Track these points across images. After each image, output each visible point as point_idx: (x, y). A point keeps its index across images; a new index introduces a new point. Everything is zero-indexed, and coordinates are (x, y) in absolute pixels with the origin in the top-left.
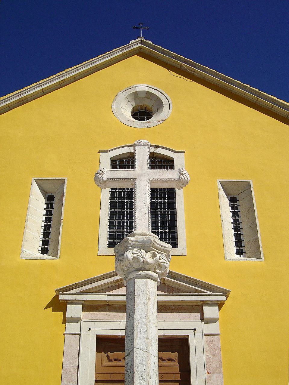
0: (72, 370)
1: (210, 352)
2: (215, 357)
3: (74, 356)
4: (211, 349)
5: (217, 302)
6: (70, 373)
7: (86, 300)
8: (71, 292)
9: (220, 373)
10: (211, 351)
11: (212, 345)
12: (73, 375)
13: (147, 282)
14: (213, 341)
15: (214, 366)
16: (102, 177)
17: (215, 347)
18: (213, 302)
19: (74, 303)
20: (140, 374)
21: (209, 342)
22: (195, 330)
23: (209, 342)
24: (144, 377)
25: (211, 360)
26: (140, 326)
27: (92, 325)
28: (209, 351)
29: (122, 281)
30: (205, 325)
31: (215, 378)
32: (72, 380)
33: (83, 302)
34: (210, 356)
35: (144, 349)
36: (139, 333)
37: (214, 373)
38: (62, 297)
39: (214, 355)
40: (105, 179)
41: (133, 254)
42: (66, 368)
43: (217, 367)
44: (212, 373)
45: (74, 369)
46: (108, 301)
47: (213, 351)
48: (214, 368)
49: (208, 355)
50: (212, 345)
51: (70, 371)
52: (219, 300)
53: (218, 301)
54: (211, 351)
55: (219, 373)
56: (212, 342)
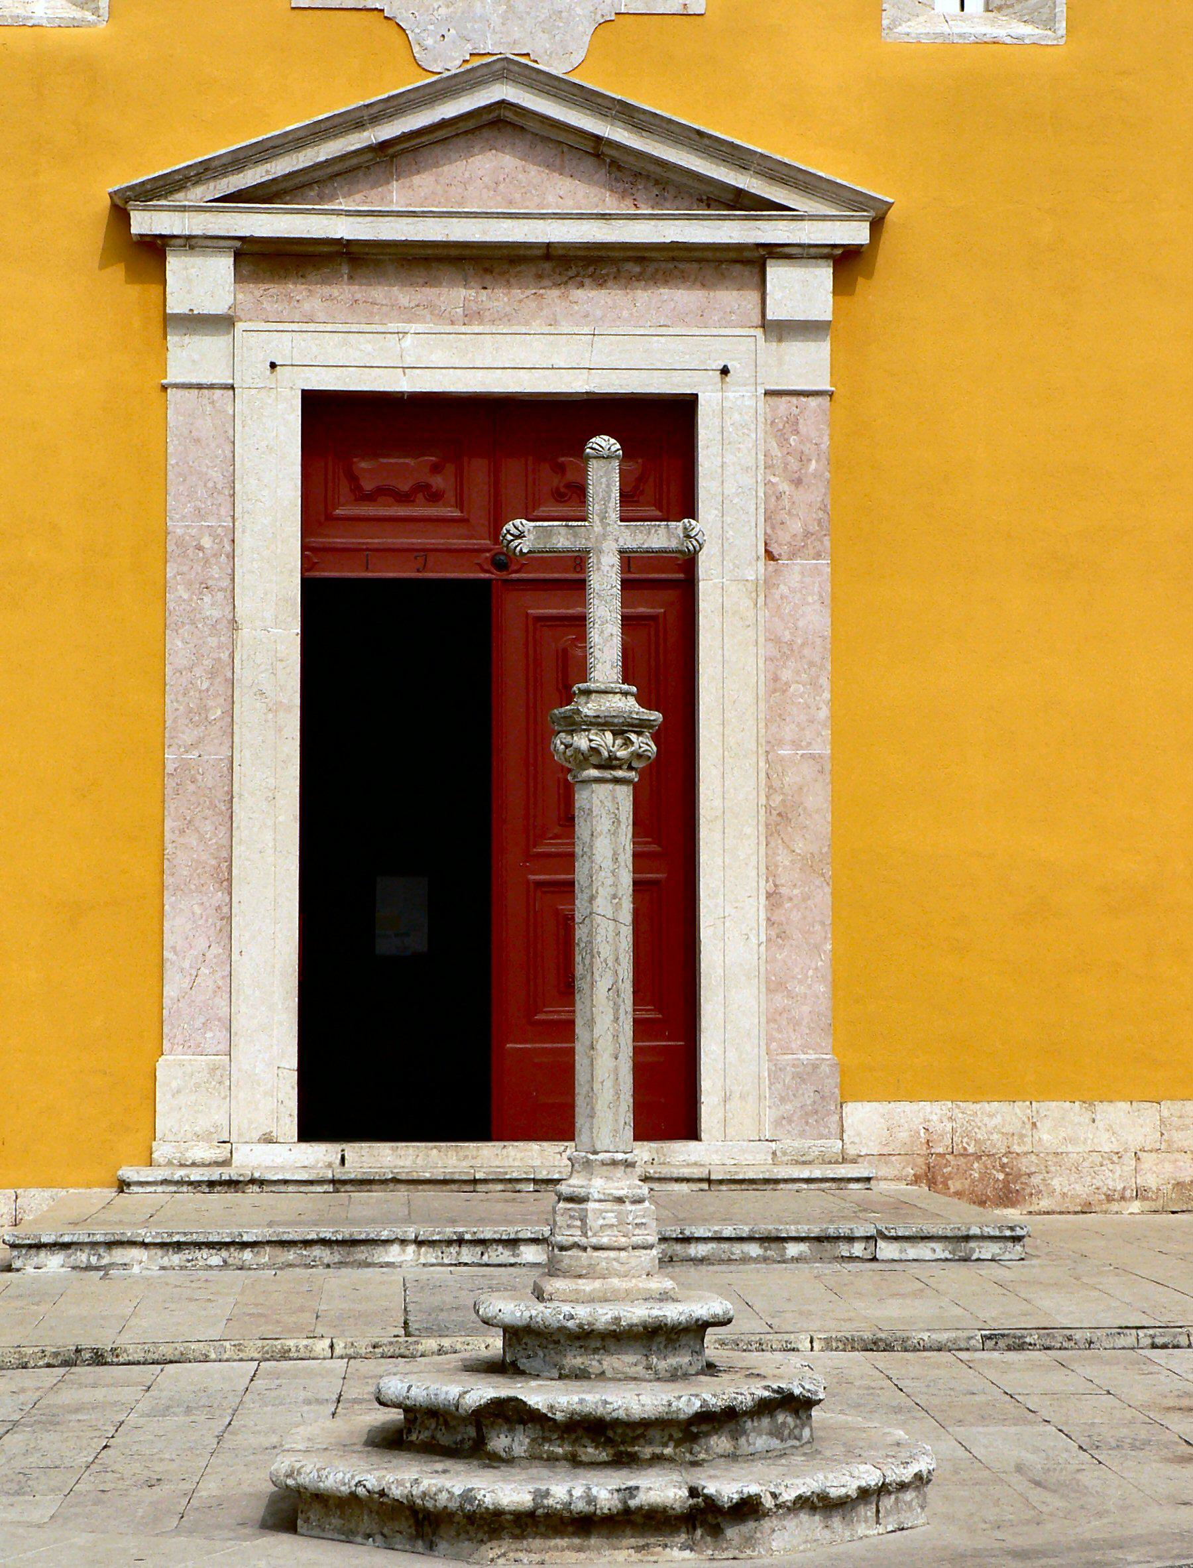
0: (206, 542)
1: (785, 469)
2: (801, 489)
3: (210, 484)
4: (789, 458)
5: (826, 251)
6: (201, 554)
7: (252, 236)
8: (181, 198)
9: (818, 556)
10: (786, 465)
11: (793, 440)
12: (213, 560)
13: (614, 790)
14: (801, 421)
15: (796, 526)
16: (518, 548)
17: (808, 448)
18: (813, 251)
19: (190, 243)
20: (602, 959)
21: (781, 426)
22: (725, 371)
23: (781, 426)
24: (610, 964)
25: (786, 502)
26: (603, 874)
27: (282, 346)
28: (778, 462)
29: (530, 619)
30: (768, 350)
31: (797, 577)
32: (210, 583)
33: (238, 244)
34: (785, 487)
35: (610, 916)
36: (600, 888)
37: (792, 556)
38: (143, 222)
39: (798, 482)
40: (525, 550)
41: (591, 741)
42: (179, 531)
43: (807, 534)
44: (784, 556)
45: (215, 537)
46: (347, 240)
47: (794, 464)
48: (795, 535)
49: (774, 480)
50: (793, 440)
51: (200, 548)
52: (838, 242)
53: (834, 246)
54: (786, 465)
55: (814, 559)
56: (793, 423)
